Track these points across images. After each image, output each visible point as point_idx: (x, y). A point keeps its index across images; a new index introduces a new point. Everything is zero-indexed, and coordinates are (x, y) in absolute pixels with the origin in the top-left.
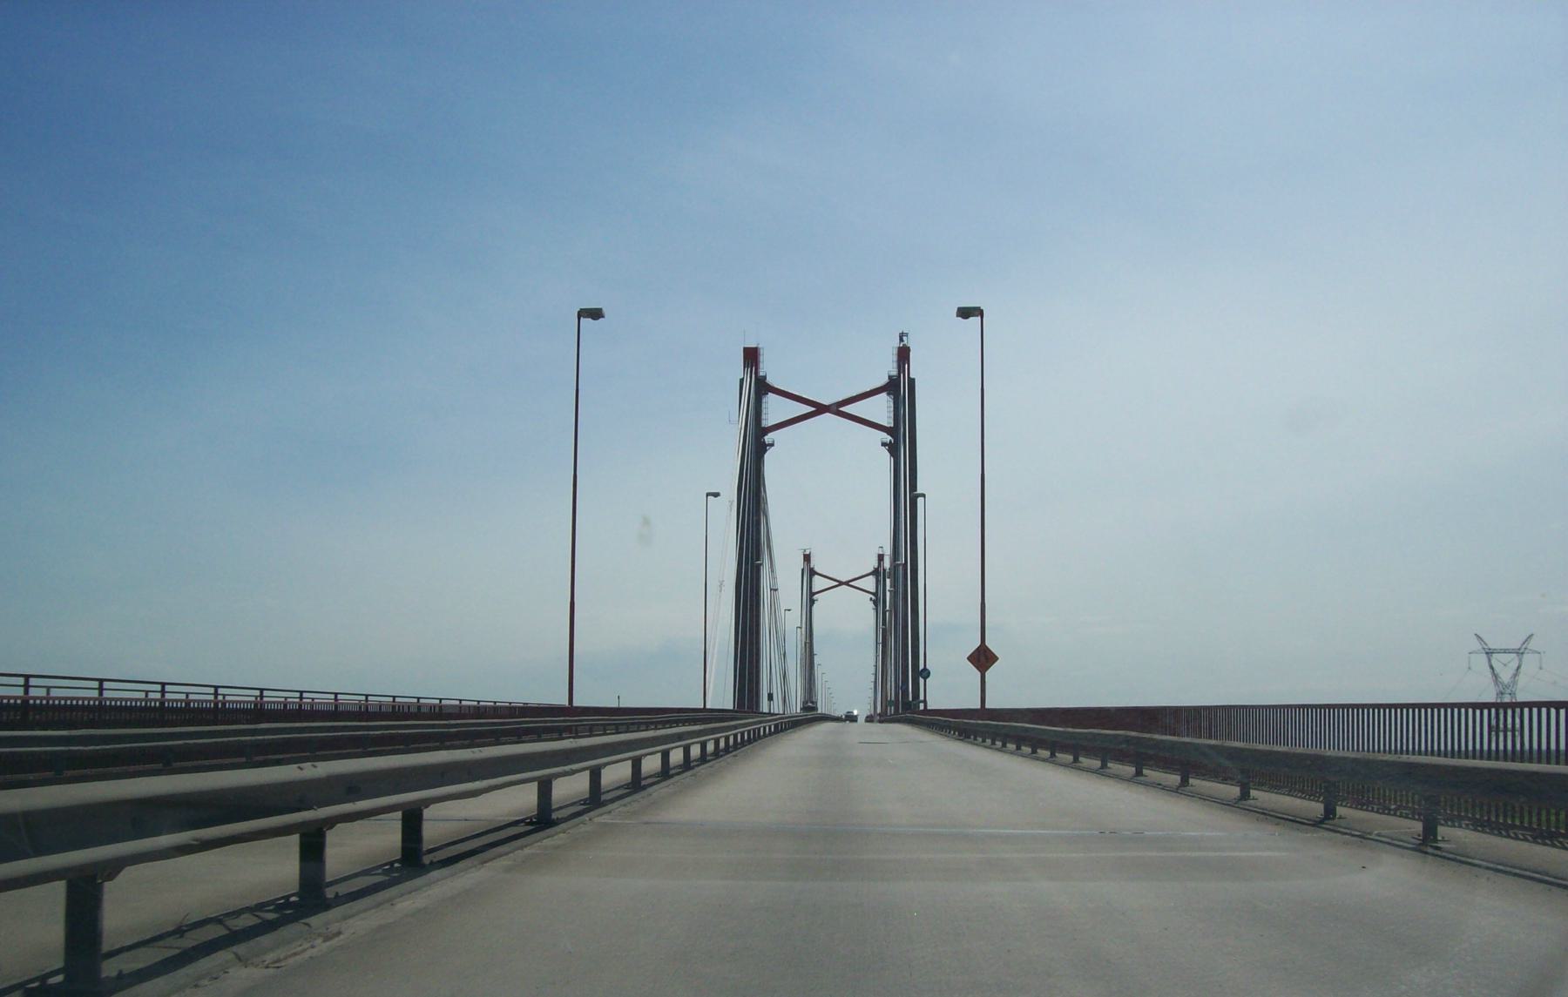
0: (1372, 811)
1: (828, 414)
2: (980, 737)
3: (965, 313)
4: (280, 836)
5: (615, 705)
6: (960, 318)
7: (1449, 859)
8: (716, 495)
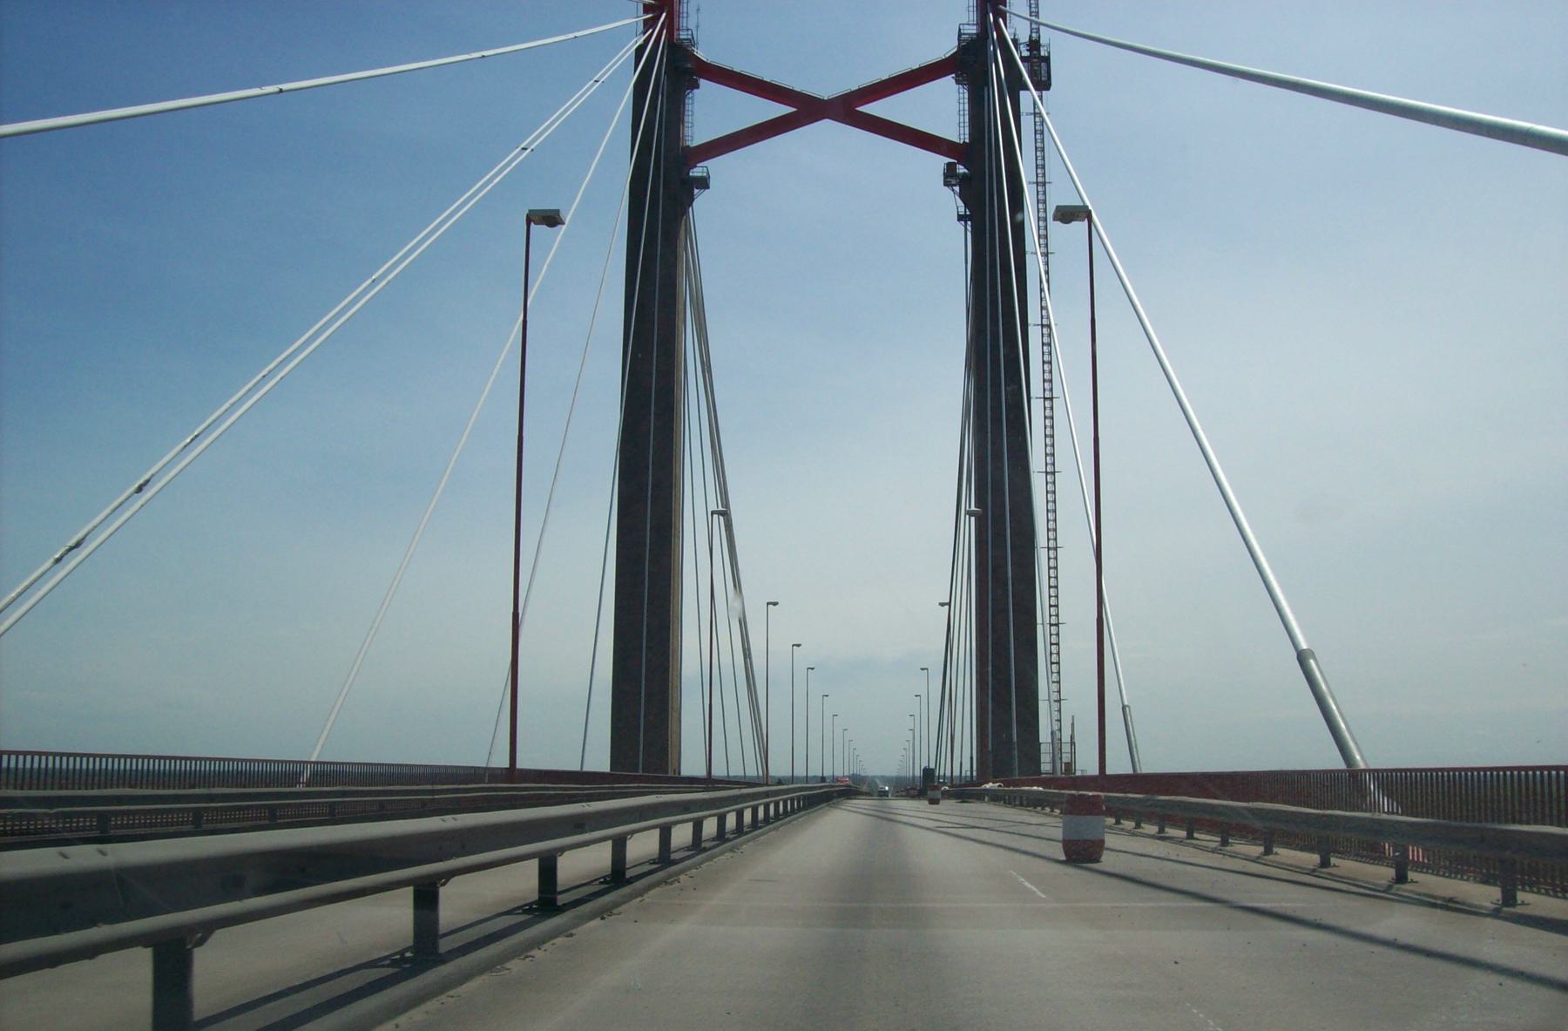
1: (826, 120)
2: (1057, 808)
4: (289, 913)
5: (573, 765)
6: (1059, 223)
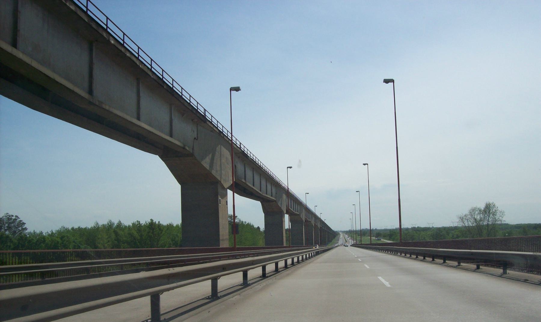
0: (516, 271)
3: (387, 81)
6: (385, 83)
7: (514, 280)
8: (291, 167)
